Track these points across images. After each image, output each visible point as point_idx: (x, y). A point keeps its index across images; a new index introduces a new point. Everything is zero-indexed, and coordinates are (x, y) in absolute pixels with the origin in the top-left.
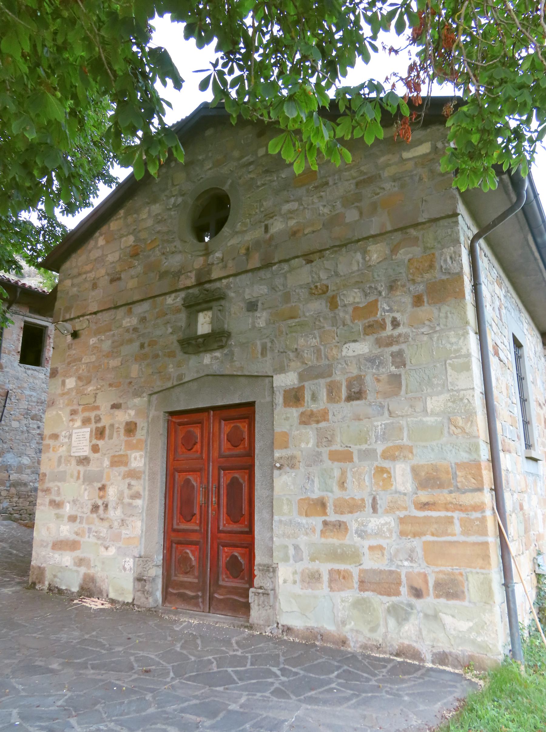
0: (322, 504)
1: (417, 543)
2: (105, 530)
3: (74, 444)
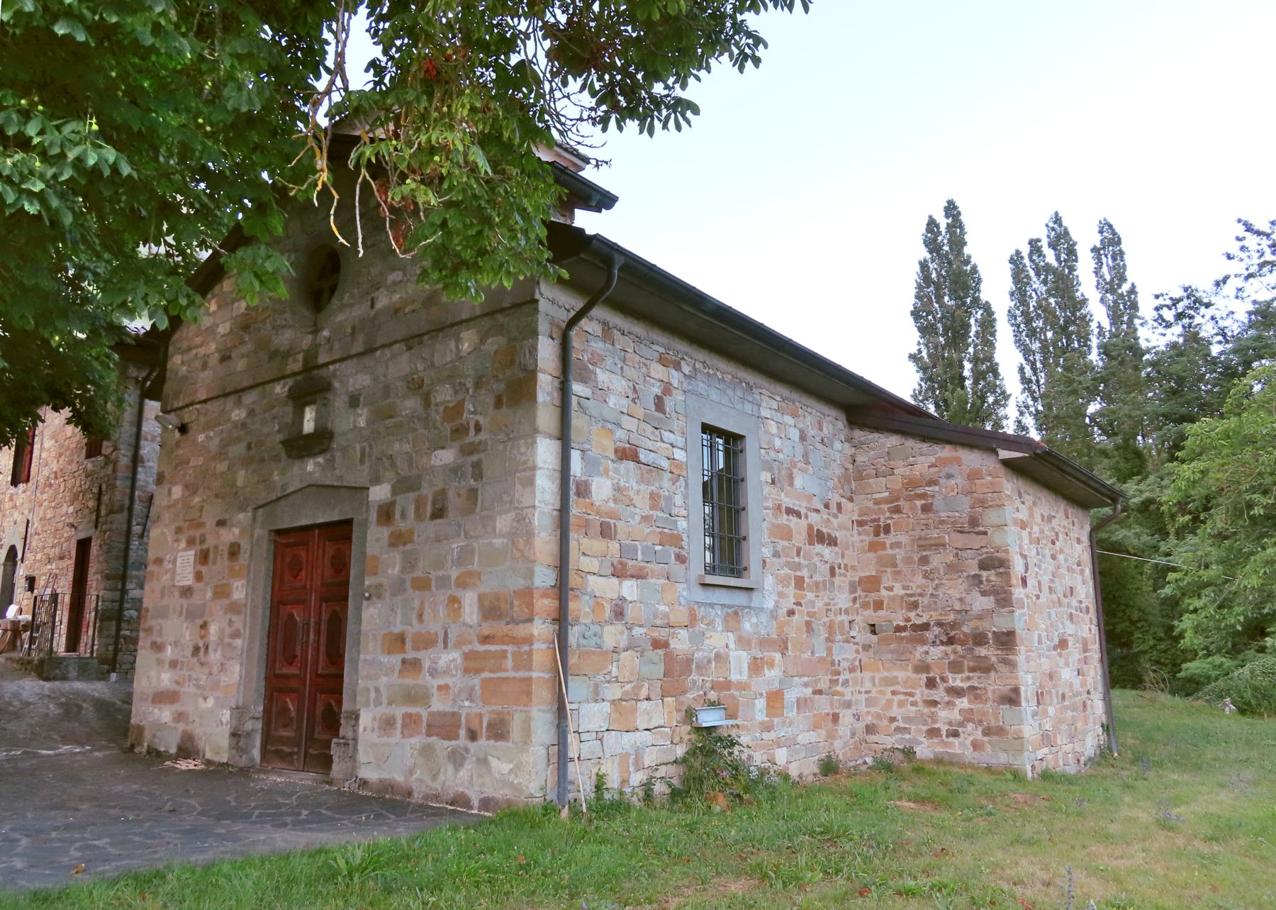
0: (401, 639)
1: (476, 681)
2: (204, 678)
3: (179, 570)
